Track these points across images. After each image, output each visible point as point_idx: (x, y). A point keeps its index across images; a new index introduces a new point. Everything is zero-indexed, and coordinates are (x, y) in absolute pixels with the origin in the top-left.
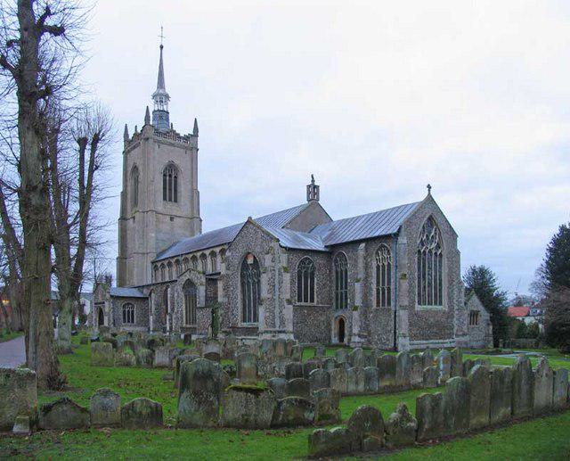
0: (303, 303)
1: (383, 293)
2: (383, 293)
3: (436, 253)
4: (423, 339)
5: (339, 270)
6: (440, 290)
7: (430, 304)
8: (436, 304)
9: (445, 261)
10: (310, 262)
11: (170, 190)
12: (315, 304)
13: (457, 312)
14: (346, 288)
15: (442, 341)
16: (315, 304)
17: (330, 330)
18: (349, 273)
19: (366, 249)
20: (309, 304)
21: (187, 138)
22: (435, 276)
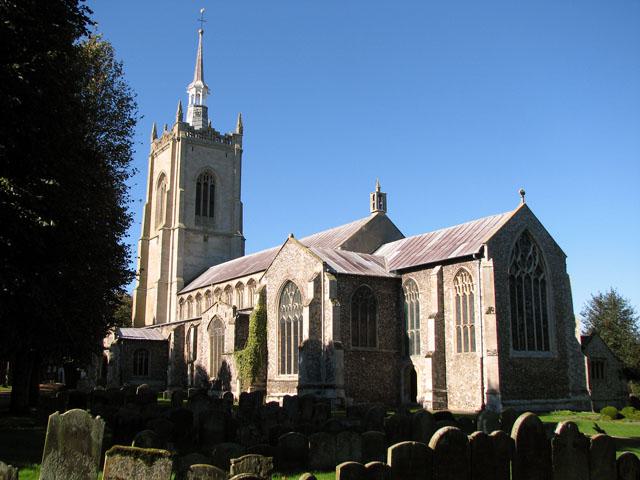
0: (360, 348)
1: (466, 333)
2: (466, 333)
3: (536, 280)
4: (524, 399)
5: (461, 295)
6: (546, 330)
7: (531, 348)
8: (540, 348)
9: (549, 290)
10: (370, 292)
11: (205, 201)
12: (377, 348)
13: (571, 360)
14: (418, 326)
15: (552, 400)
16: (377, 348)
17: (398, 385)
18: (421, 307)
19: (440, 275)
20: (368, 349)
21: (228, 139)
22: (538, 310)
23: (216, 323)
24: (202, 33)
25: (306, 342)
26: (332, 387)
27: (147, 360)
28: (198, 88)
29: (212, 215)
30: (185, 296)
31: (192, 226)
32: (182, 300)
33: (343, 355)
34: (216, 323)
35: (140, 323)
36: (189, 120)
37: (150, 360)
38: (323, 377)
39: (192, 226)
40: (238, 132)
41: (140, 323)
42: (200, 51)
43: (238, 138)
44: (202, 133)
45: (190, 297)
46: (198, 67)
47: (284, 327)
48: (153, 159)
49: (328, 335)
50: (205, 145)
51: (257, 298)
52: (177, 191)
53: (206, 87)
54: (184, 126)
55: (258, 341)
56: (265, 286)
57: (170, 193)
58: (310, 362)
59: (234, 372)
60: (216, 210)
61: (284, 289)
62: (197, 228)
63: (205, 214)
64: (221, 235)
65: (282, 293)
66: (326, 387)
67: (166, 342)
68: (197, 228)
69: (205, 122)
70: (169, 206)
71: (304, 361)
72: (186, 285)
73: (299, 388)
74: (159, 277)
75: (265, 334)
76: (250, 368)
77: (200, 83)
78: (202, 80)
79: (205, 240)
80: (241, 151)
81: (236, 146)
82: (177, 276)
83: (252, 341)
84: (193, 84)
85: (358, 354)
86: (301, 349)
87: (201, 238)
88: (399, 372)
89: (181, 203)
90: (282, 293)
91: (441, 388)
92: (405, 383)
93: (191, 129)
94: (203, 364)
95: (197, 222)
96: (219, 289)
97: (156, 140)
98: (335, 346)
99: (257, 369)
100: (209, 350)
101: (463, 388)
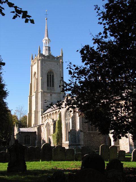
0: (91, 132)
11: (50, 81)
20: (94, 132)
21: (58, 58)
23: (48, 124)
24: (47, 19)
25: (71, 131)
26: (80, 145)
27: (29, 139)
28: (46, 40)
29: (53, 86)
30: (43, 116)
31: (46, 90)
32: (43, 117)
33: (83, 135)
34: (48, 124)
35: (30, 126)
36: (44, 53)
37: (30, 139)
38: (77, 142)
39: (46, 90)
40: (61, 55)
41: (30, 126)
42: (46, 26)
43: (61, 57)
44: (48, 57)
45: (45, 116)
46: (46, 32)
47: (67, 125)
48: (32, 67)
49: (78, 128)
50: (50, 61)
51: (58, 116)
52: (40, 78)
53: (49, 39)
54: (41, 55)
55: (59, 130)
56: (61, 112)
57: (37, 79)
58: (72, 137)
59: (52, 141)
60: (55, 84)
61: (66, 113)
62: (48, 91)
63: (50, 86)
64: (57, 93)
65: (66, 114)
66: (78, 145)
67: (36, 132)
68: (48, 91)
69: (49, 53)
70: (37, 84)
71: (70, 136)
72: (44, 112)
73: (69, 146)
74: (35, 110)
75: (61, 128)
76: (56, 140)
77: (47, 38)
78: (48, 37)
79: (51, 95)
80: (63, 62)
81: (61, 60)
82: (41, 109)
83: (57, 130)
84: (44, 39)
85: (90, 133)
86: (69, 132)
87: (49, 95)
88: (106, 140)
89: (41, 83)
90: (66, 114)
91: (117, 145)
92: (108, 143)
93: (44, 56)
94: (45, 139)
95: (48, 89)
96: (53, 113)
97: (33, 60)
98: (80, 131)
99: (59, 140)
100: (46, 133)
101: (124, 144)
